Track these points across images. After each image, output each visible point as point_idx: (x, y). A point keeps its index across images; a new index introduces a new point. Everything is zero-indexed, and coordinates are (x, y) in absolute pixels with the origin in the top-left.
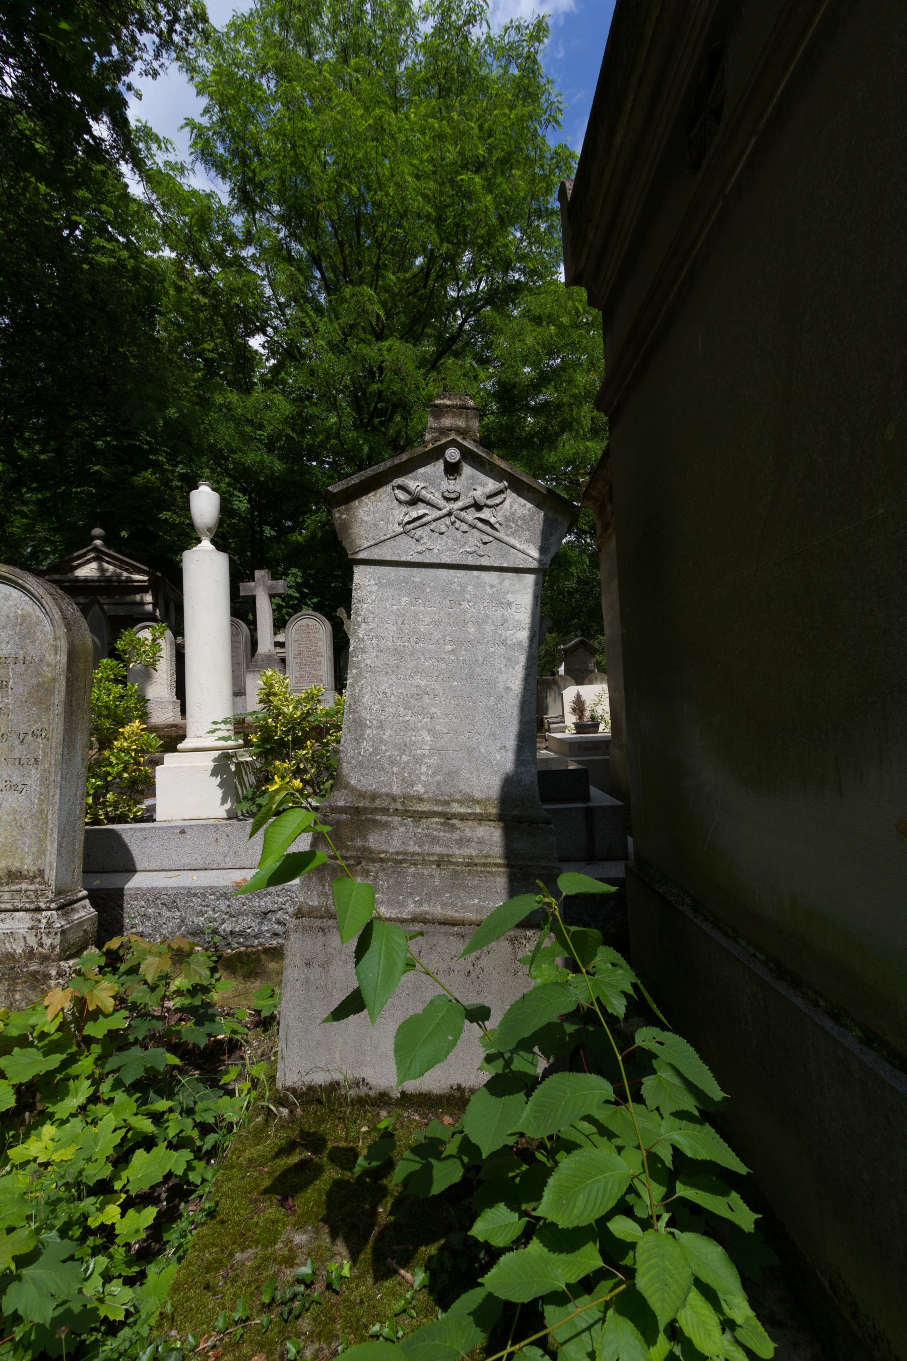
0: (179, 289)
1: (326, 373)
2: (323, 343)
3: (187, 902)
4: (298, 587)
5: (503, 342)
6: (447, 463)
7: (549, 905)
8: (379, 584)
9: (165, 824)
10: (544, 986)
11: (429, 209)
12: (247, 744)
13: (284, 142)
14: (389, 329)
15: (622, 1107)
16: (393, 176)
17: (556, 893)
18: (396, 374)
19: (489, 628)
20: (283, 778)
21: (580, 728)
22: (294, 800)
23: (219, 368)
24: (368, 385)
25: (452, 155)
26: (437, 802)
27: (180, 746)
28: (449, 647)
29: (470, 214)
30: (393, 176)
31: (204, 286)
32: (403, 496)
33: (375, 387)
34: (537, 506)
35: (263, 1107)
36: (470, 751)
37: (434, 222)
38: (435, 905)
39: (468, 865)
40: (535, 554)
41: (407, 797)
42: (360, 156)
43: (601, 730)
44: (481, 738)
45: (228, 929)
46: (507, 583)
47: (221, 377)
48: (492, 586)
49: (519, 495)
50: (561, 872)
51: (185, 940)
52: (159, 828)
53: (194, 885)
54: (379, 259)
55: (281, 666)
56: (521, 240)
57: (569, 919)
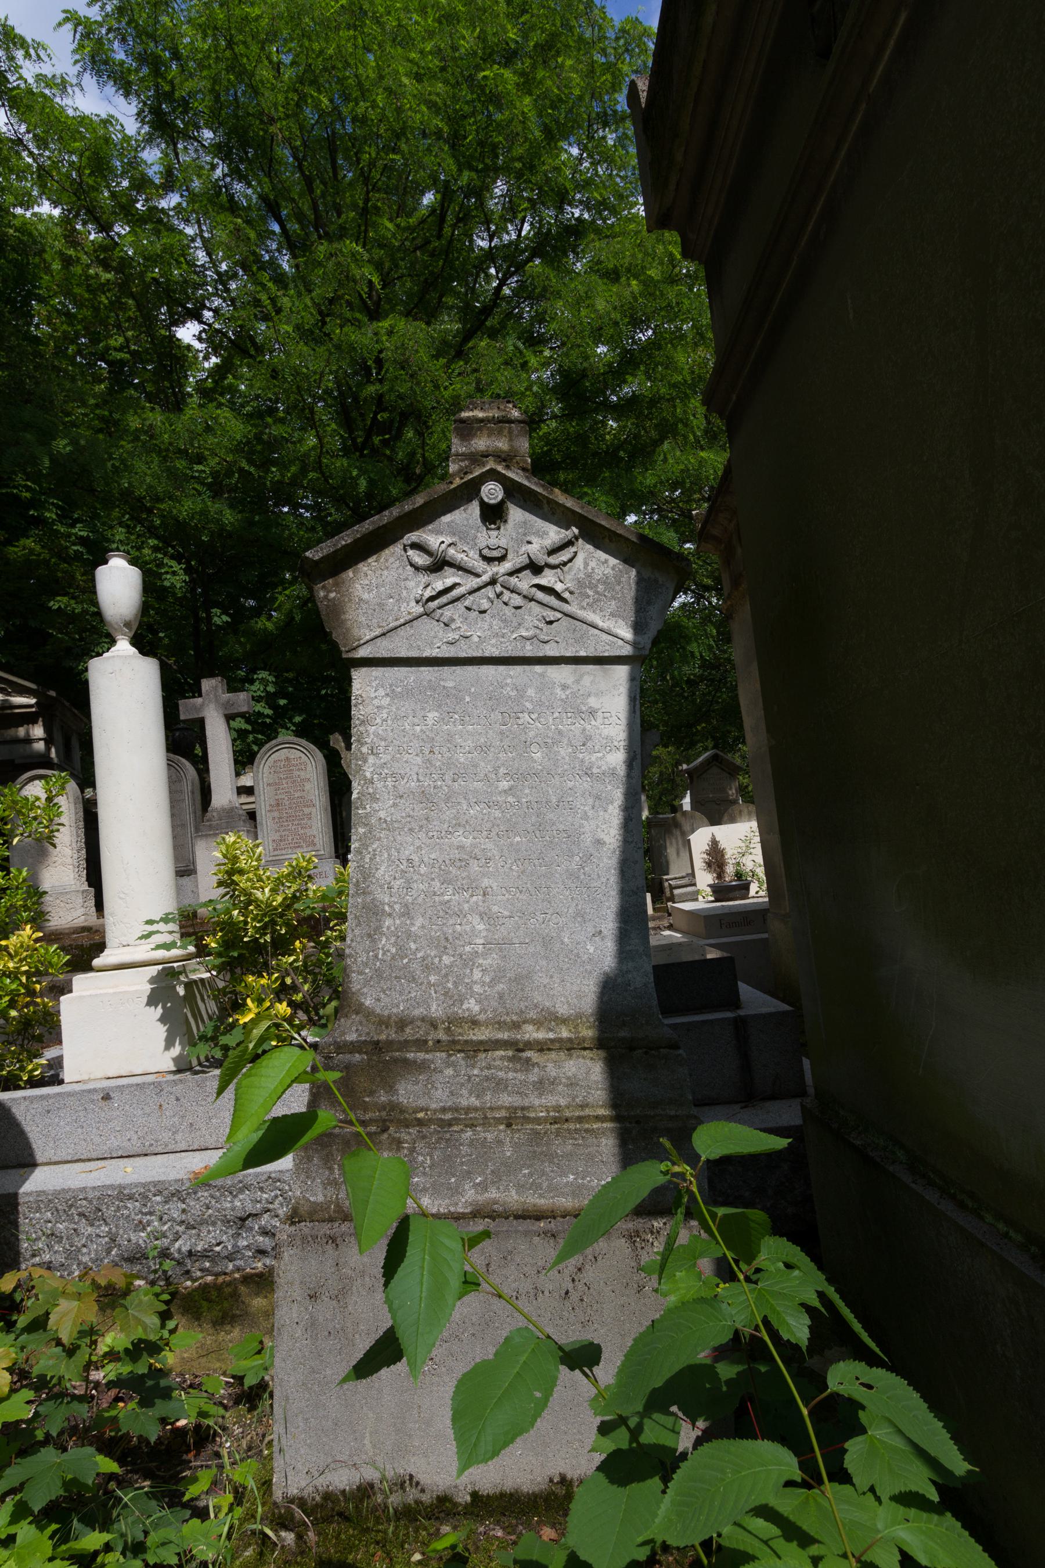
0: (68, 262)
1: (296, 373)
2: (290, 329)
3: (118, 1209)
4: (270, 699)
5: (561, 310)
6: (484, 505)
7: (682, 1176)
8: (392, 694)
9: (77, 1087)
10: (683, 1305)
11: (438, 122)
12: (202, 951)
13: (215, 38)
14: (389, 301)
15: (816, 1491)
16: (381, 77)
17: (692, 1158)
18: (403, 368)
19: (564, 751)
20: (260, 1001)
21: (720, 892)
22: (280, 1034)
23: (133, 374)
24: (360, 385)
25: (467, 40)
26: (501, 1025)
27: (96, 962)
28: (504, 785)
29: (500, 127)
30: (381, 77)
31: (105, 254)
32: (420, 559)
33: (371, 389)
34: (625, 561)
35: (253, 1532)
36: (547, 942)
37: (446, 141)
38: (507, 1189)
39: (555, 1121)
40: (627, 634)
41: (454, 1021)
42: (331, 51)
43: (752, 893)
44: (562, 920)
45: (184, 1249)
46: (587, 681)
47: (136, 387)
48: (564, 687)
49: (597, 546)
50: (701, 1123)
51: (118, 1271)
52: (70, 1094)
53: (128, 1180)
54: (367, 200)
55: (248, 826)
56: (580, 160)
57: (716, 1195)
